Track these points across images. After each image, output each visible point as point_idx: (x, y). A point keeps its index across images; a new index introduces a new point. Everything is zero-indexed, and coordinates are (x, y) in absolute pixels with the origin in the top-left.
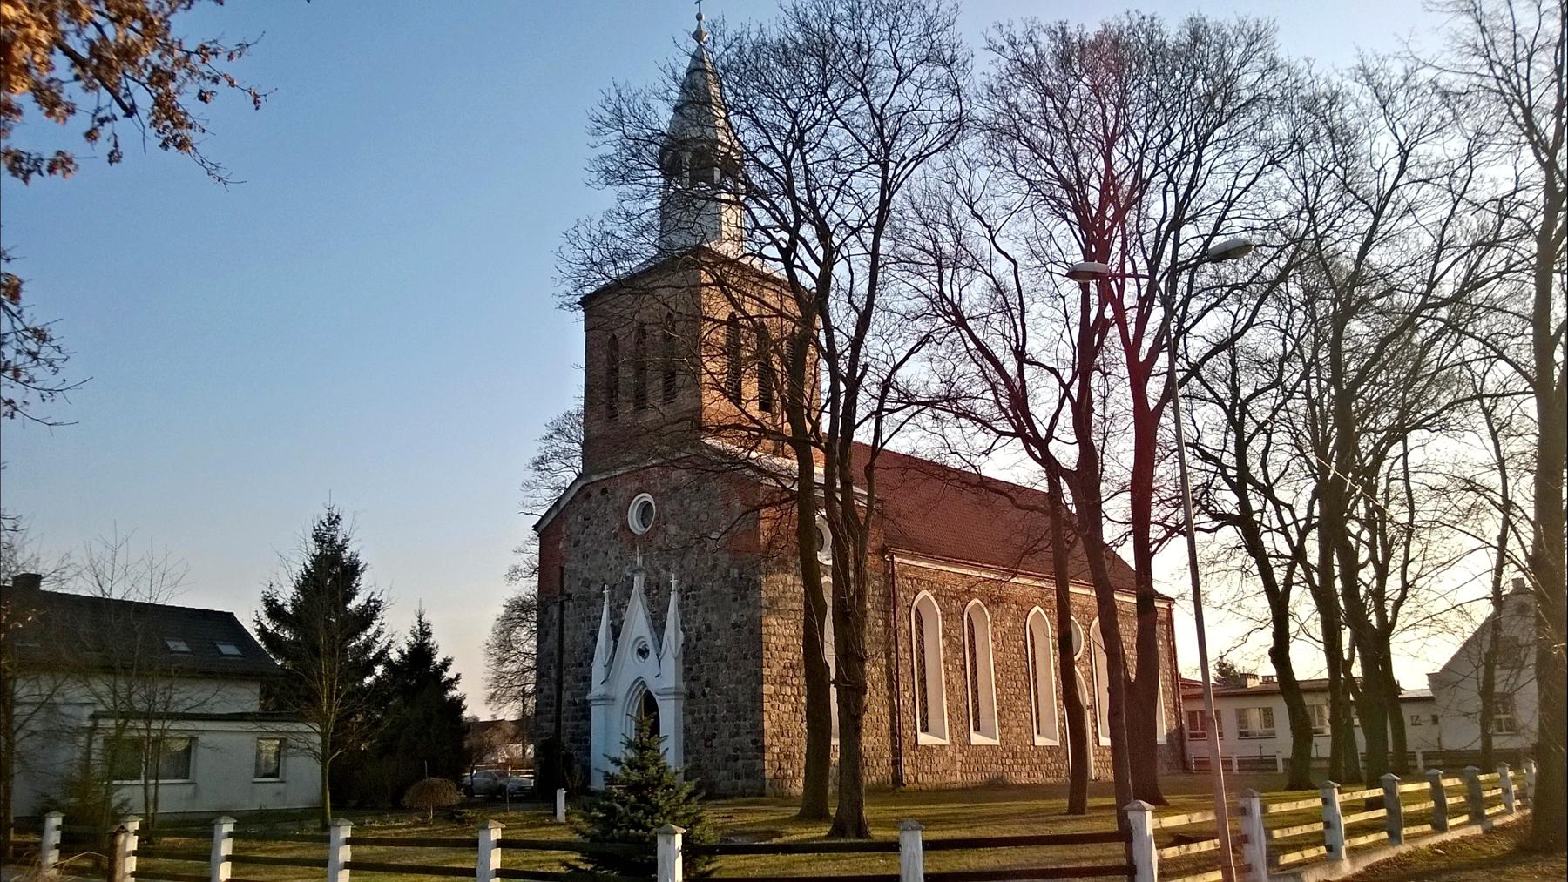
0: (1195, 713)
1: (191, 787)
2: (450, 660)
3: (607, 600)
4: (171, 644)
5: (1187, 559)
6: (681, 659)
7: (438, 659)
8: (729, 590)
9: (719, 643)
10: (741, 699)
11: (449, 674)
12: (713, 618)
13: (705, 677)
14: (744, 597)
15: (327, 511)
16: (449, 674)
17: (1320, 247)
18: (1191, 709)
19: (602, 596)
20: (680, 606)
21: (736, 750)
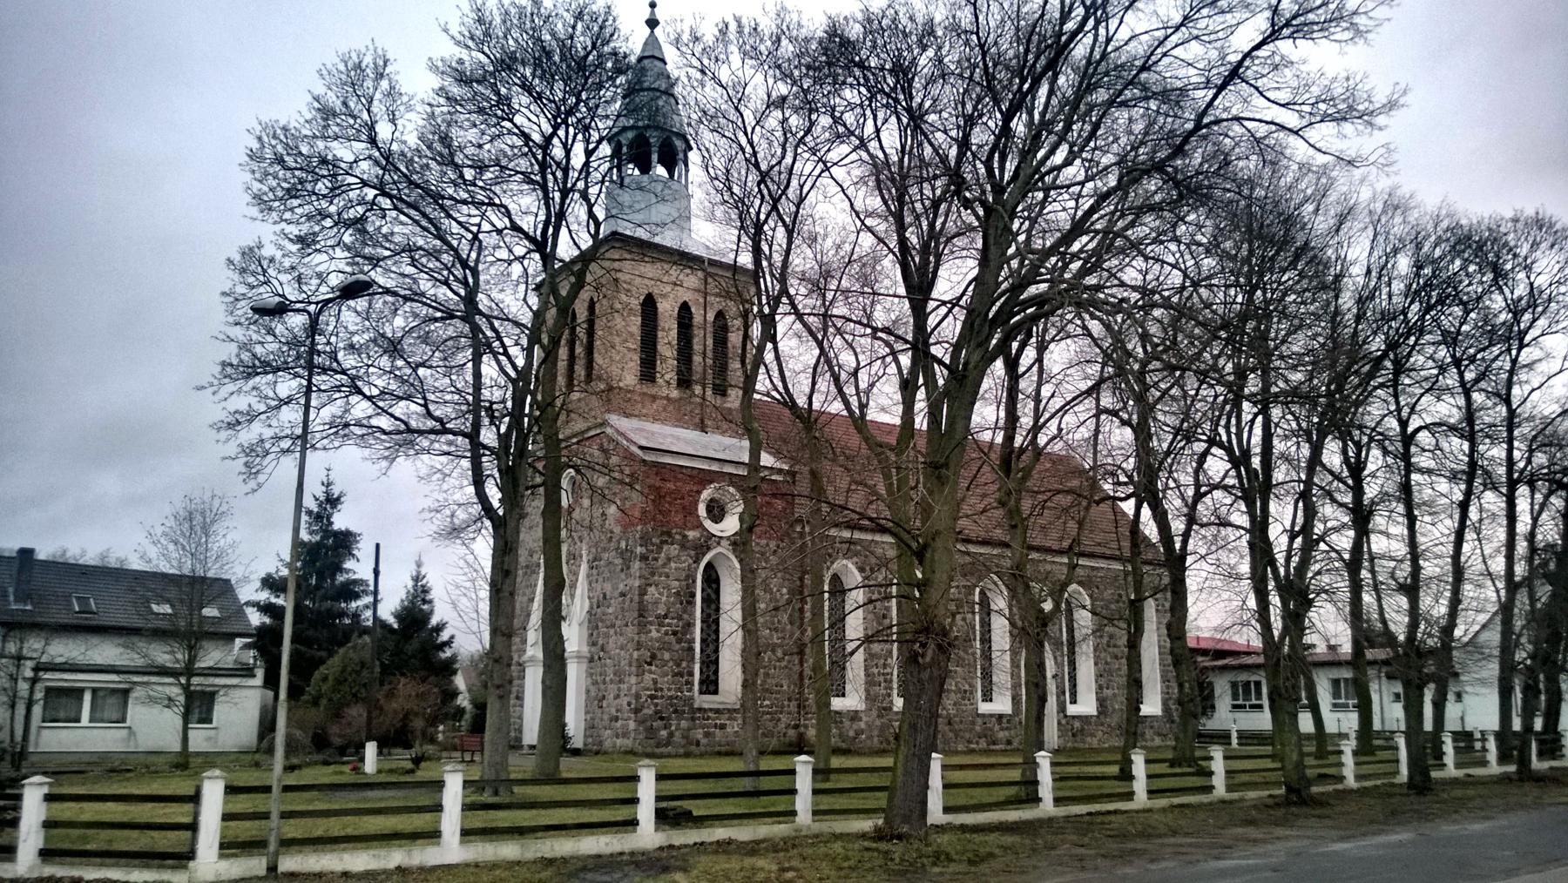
0: (1249, 682)
1: (126, 731)
2: (444, 625)
3: (542, 569)
4: (155, 607)
5: (380, 578)
6: (586, 624)
7: (434, 621)
8: (618, 561)
9: (610, 610)
10: (623, 663)
11: (444, 636)
12: (608, 587)
13: (600, 642)
14: (628, 568)
15: (324, 489)
16: (444, 636)
17: (1043, 208)
18: (1336, 677)
19: (539, 565)
20: (588, 576)
21: (617, 711)
